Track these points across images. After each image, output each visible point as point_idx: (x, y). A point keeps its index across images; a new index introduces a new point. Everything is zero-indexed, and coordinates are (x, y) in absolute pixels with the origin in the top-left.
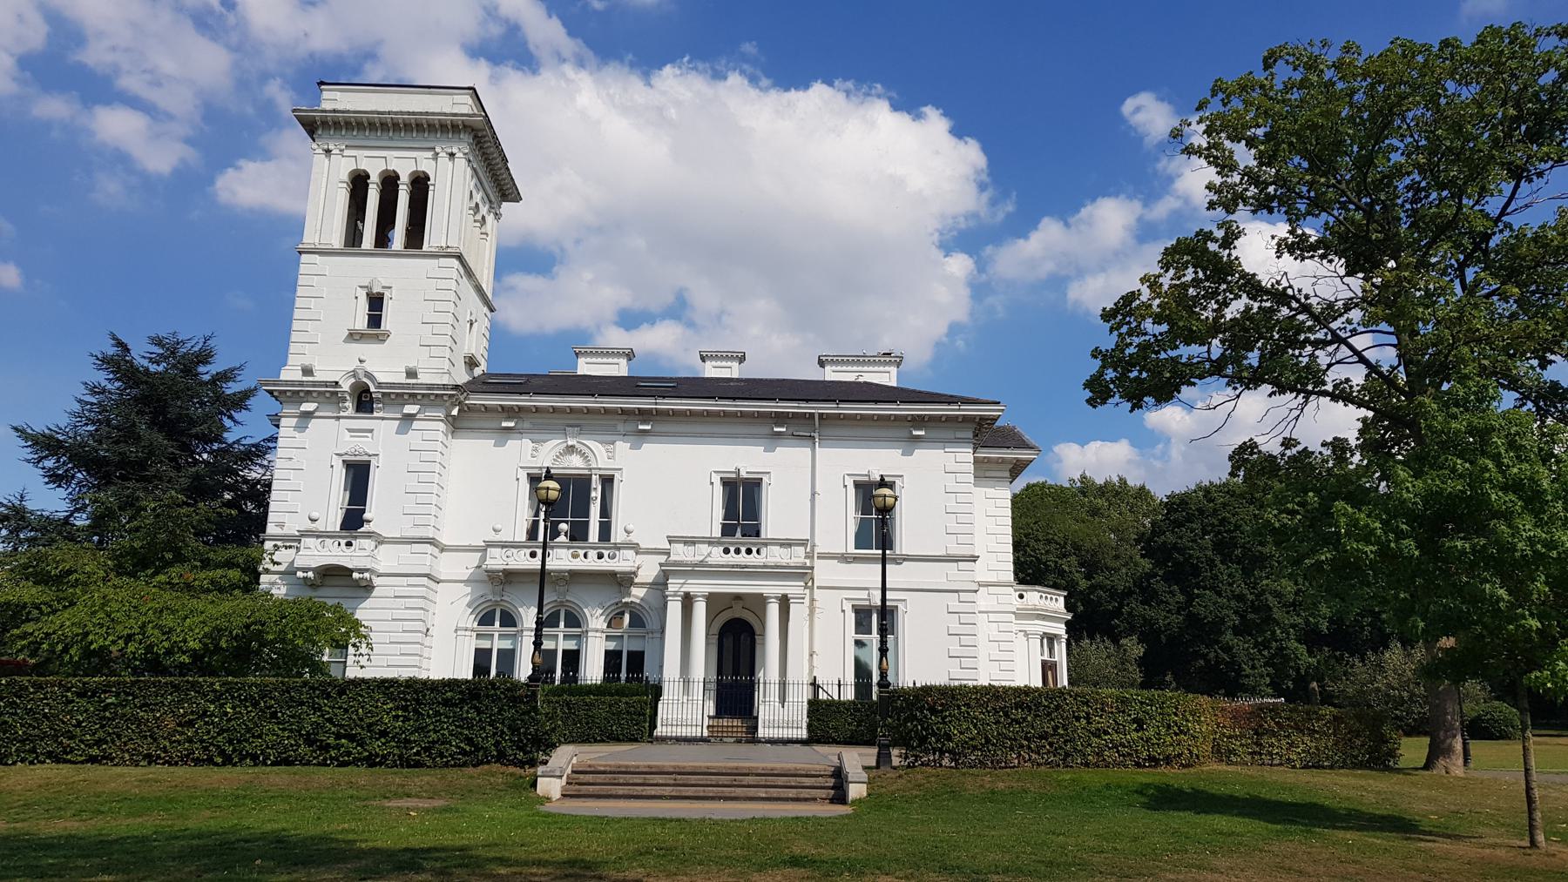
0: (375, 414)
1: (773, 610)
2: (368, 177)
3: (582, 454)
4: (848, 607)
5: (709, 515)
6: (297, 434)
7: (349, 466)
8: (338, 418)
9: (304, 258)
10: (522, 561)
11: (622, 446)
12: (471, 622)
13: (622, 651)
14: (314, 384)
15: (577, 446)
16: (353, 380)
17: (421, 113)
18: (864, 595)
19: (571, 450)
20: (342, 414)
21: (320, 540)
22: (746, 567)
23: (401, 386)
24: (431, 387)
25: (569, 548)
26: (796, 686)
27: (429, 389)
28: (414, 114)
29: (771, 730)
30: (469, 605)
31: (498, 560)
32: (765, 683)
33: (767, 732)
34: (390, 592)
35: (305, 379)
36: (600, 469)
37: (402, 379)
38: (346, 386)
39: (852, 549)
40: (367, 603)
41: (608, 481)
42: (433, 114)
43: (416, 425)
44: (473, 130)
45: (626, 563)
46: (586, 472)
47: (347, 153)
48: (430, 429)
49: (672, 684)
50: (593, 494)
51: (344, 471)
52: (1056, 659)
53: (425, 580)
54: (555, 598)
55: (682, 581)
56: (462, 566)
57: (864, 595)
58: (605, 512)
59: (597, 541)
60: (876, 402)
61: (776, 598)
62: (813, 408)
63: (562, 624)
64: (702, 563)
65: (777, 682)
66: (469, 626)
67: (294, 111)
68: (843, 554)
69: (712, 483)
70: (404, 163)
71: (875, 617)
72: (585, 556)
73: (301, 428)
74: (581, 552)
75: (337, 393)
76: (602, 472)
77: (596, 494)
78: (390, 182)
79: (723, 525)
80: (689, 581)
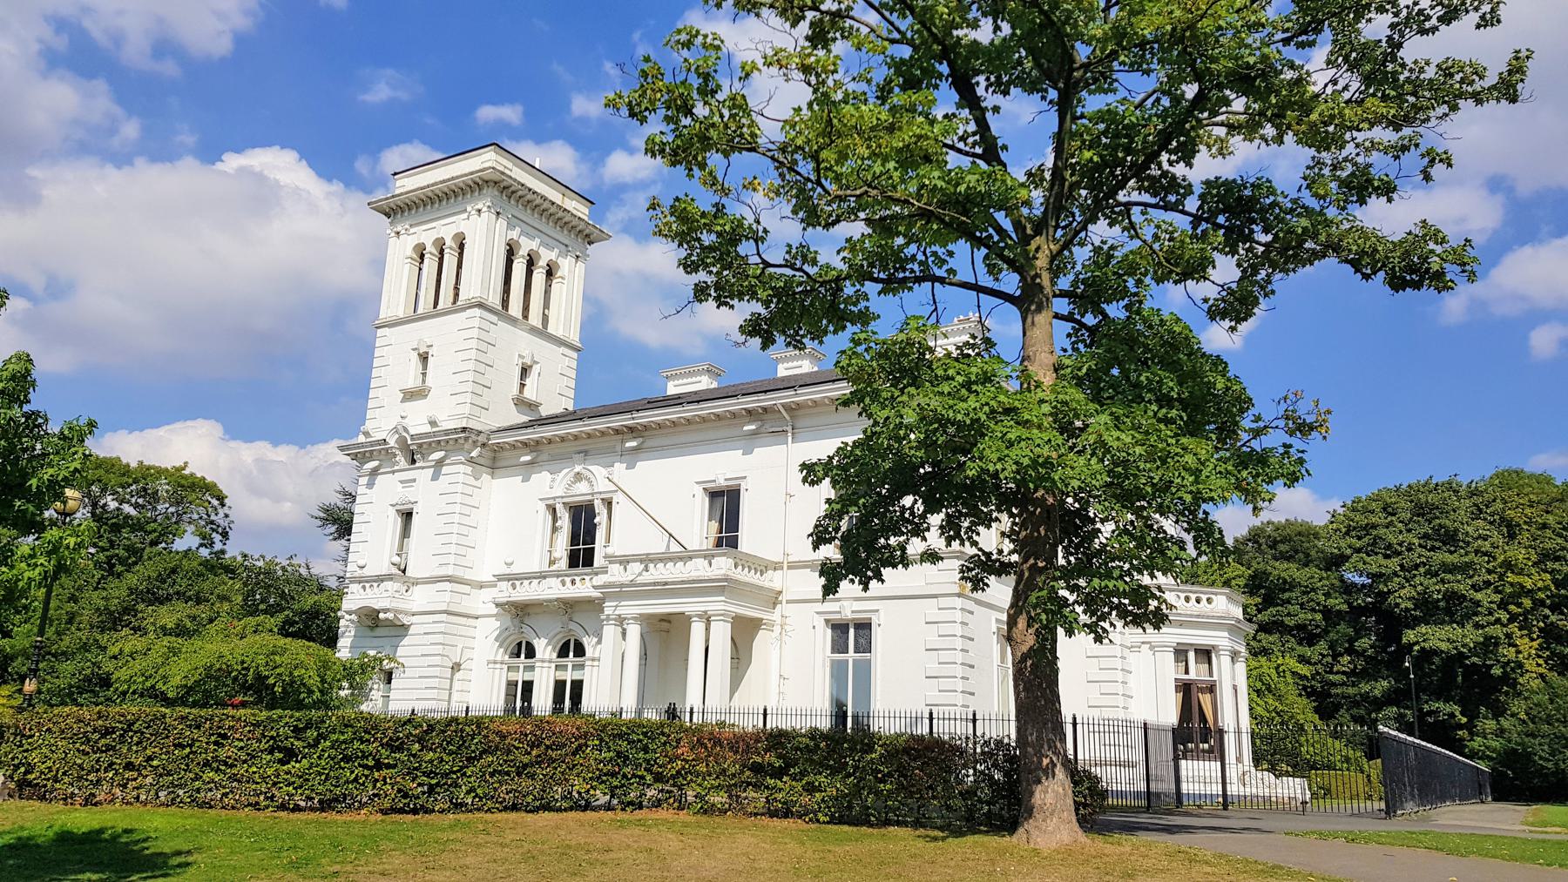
0: (417, 465)
1: (697, 629)
3: (588, 480)
4: (820, 622)
5: (698, 528)
6: (368, 491)
7: (714, 495)
8: (393, 472)
9: (380, 332)
10: (553, 589)
11: (619, 468)
12: (501, 655)
13: (517, 682)
14: (372, 444)
15: (584, 471)
16: (397, 436)
17: (449, 180)
19: (578, 477)
20: (396, 468)
21: (560, 579)
22: (666, 584)
23: (427, 435)
24: (447, 432)
26: (987, 722)
27: (446, 435)
28: (444, 181)
29: (1197, 785)
30: (496, 640)
31: (527, 592)
33: (1208, 788)
34: (422, 629)
35: (434, 430)
36: (600, 493)
37: (428, 428)
38: (392, 442)
40: (406, 641)
42: (457, 177)
43: (445, 470)
44: (496, 183)
45: (550, 591)
46: (590, 497)
47: (412, 230)
48: (457, 471)
51: (707, 499)
52: (1215, 678)
53: (444, 617)
54: (559, 629)
55: (615, 604)
56: (483, 602)
61: (633, 618)
62: (773, 399)
63: (571, 654)
64: (632, 584)
65: (829, 713)
66: (499, 658)
67: (369, 204)
71: (852, 631)
73: (370, 485)
75: (387, 450)
76: (565, 500)
80: (623, 603)
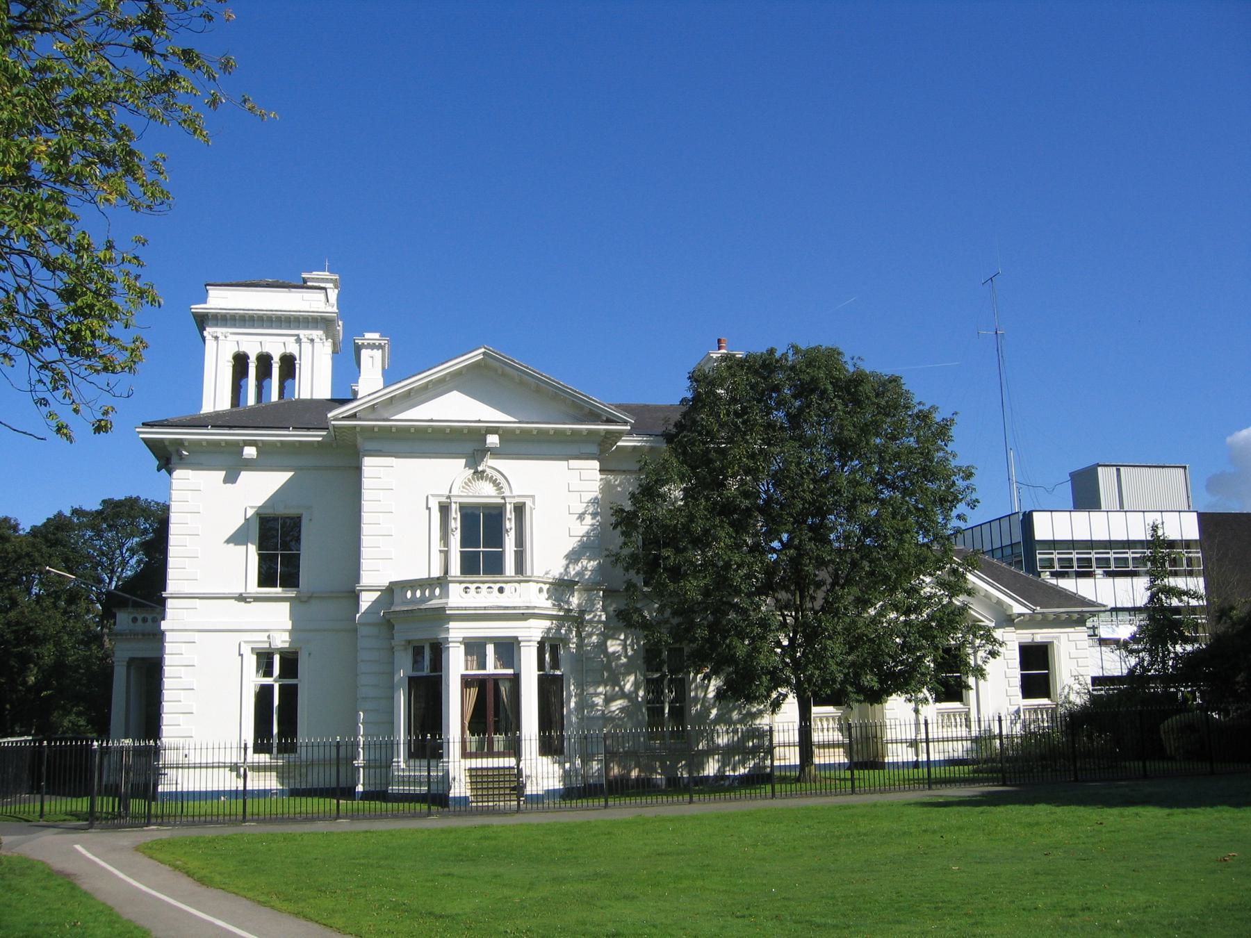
2: (272, 358)
4: (246, 650)
18: (263, 636)
25: (461, 582)
32: (240, 748)
36: (514, 497)
39: (253, 587)
41: (519, 509)
49: (903, 727)
50: (508, 525)
57: (263, 636)
58: (520, 542)
59: (513, 574)
60: (230, 427)
68: (241, 594)
69: (429, 509)
70: (276, 344)
72: (501, 590)
74: (140, 618)
77: (510, 524)
78: (264, 361)
79: (461, 552)
